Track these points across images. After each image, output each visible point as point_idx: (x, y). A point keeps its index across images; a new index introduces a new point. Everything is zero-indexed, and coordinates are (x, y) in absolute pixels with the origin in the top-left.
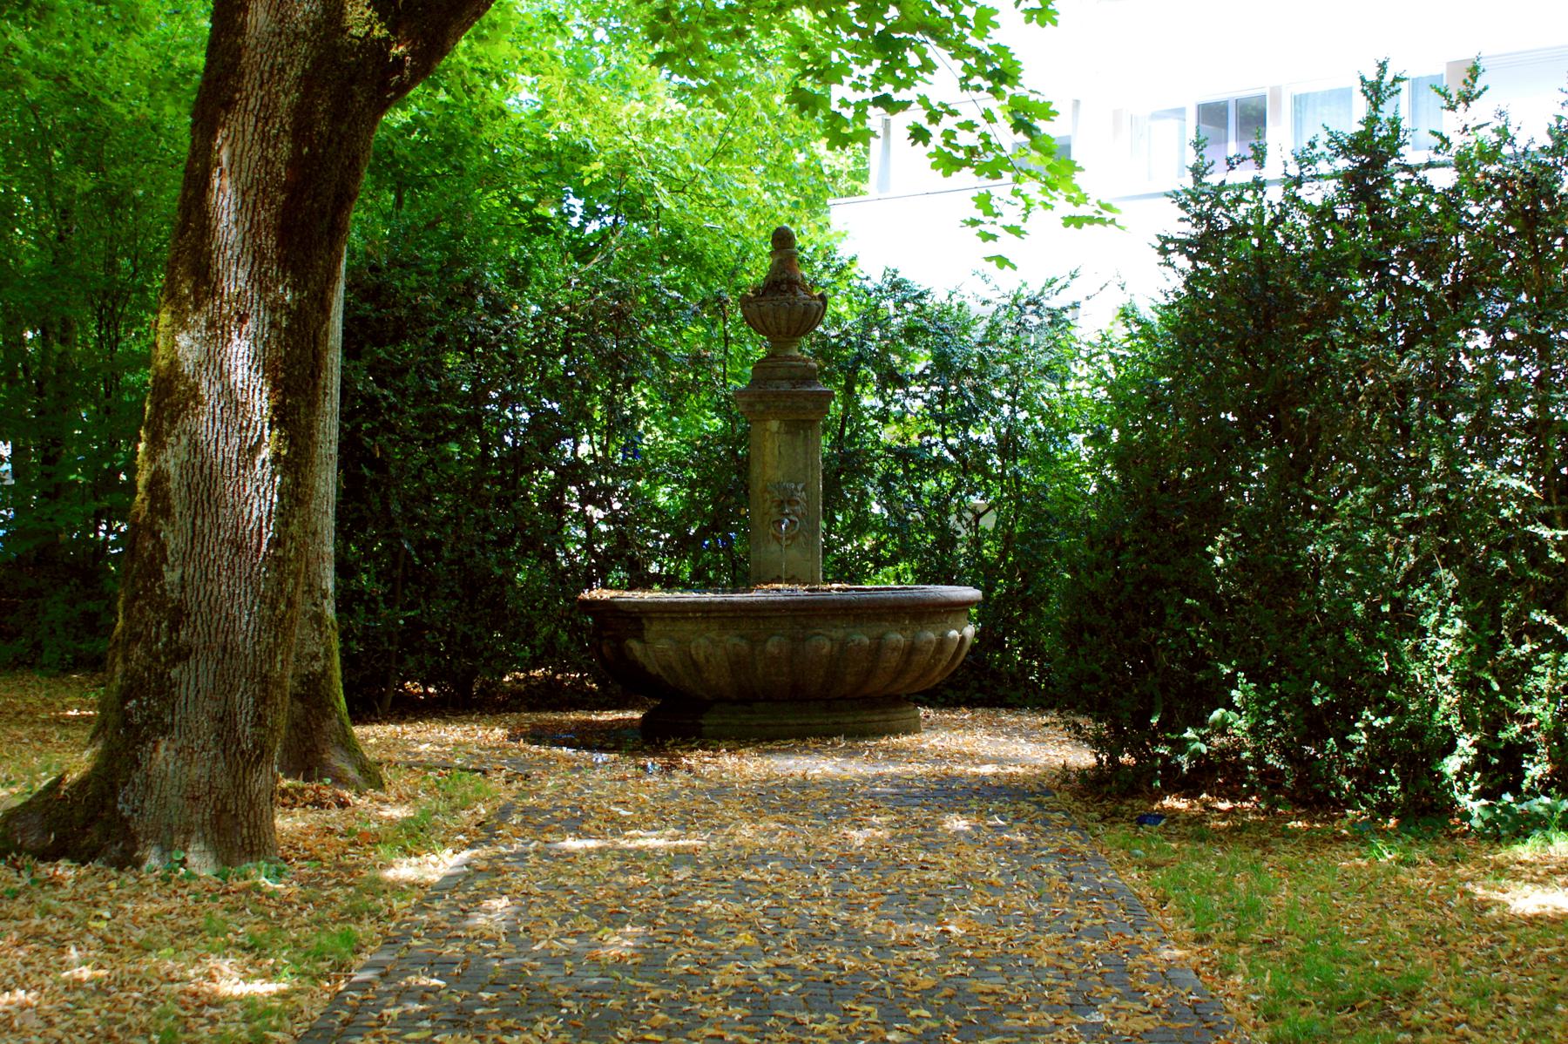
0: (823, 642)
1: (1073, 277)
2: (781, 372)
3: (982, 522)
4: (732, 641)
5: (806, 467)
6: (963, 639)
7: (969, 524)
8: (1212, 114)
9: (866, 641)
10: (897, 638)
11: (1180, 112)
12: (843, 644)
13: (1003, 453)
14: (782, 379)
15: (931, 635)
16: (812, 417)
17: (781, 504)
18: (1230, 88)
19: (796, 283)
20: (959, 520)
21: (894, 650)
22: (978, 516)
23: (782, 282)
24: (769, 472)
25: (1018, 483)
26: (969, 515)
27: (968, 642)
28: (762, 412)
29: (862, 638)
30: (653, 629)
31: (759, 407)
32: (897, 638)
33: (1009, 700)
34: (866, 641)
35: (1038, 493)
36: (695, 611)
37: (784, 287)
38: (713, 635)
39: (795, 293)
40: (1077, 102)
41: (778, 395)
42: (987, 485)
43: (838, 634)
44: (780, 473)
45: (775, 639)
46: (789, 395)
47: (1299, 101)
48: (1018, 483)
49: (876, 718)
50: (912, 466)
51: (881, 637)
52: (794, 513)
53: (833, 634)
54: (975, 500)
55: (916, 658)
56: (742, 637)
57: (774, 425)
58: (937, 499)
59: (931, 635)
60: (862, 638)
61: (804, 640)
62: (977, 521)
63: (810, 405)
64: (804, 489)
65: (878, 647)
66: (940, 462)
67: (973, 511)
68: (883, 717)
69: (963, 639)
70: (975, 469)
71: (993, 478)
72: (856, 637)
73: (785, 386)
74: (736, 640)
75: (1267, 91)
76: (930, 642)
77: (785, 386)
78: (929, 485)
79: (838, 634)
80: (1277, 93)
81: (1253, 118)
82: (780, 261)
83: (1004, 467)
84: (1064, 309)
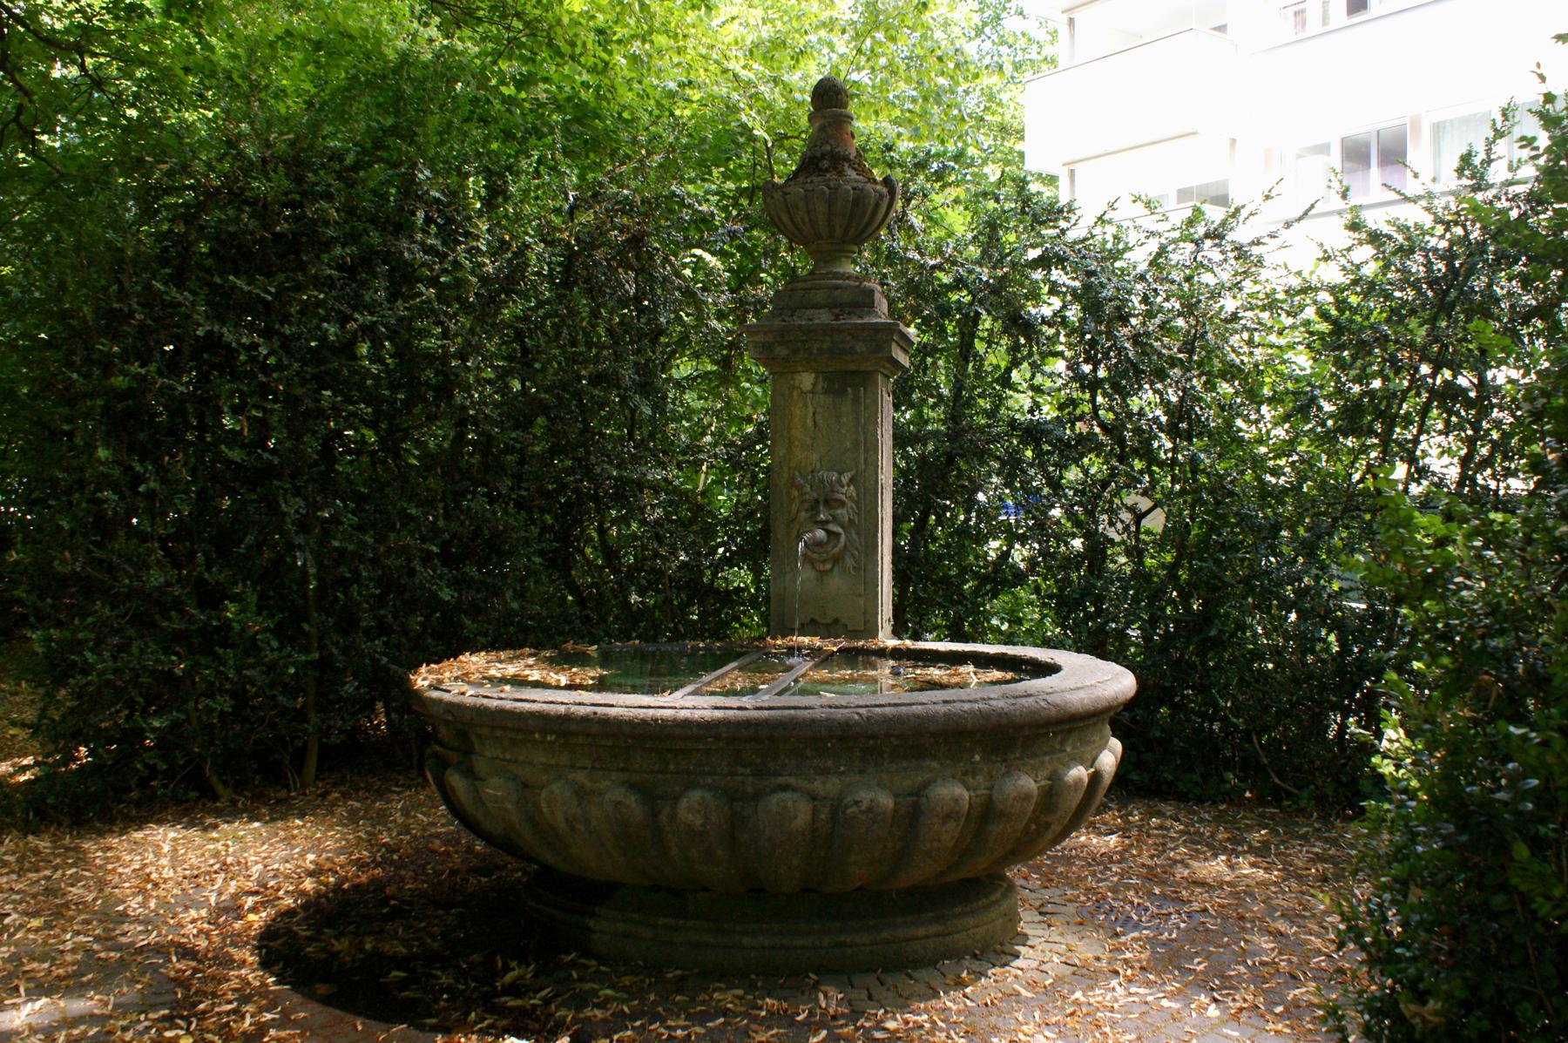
0: (791, 808)
1: (1267, 197)
2: (819, 297)
3: (1145, 523)
4: (615, 795)
5: (856, 445)
6: (1096, 777)
7: (1127, 528)
8: (1356, 154)
9: (886, 801)
10: (953, 792)
11: (1324, 149)
12: (838, 806)
13: (1172, 431)
14: (817, 307)
15: (1028, 783)
16: (866, 366)
17: (814, 506)
18: (1366, 122)
19: (846, 159)
20: (1111, 524)
21: (947, 817)
22: (1139, 517)
23: (823, 156)
24: (799, 454)
25: (1194, 471)
26: (1126, 516)
27: (1107, 779)
28: (786, 359)
29: (877, 796)
30: (487, 753)
31: (781, 351)
32: (953, 792)
33: (1181, 787)
34: (886, 801)
35: (1219, 488)
36: (544, 732)
37: (825, 164)
38: (581, 777)
39: (841, 173)
40: (1234, 141)
41: (809, 331)
42: (1151, 474)
43: (828, 786)
44: (815, 457)
45: (696, 795)
46: (828, 331)
47: (1438, 129)
48: (1194, 471)
49: (921, 931)
50: (1046, 447)
51: (918, 792)
52: (835, 519)
53: (818, 786)
54: (1131, 498)
55: (995, 829)
56: (632, 786)
57: (807, 380)
58: (1083, 493)
59: (1028, 783)
60: (877, 796)
61: (758, 796)
62: (1138, 524)
63: (860, 347)
64: (852, 481)
65: (912, 813)
66: (1085, 444)
67: (1131, 509)
68: (936, 928)
69: (1096, 777)
70: (1135, 452)
71: (1161, 464)
72: (865, 796)
73: (824, 317)
74: (618, 793)
75: (1407, 120)
76: (1027, 797)
77: (824, 317)
78: (1073, 474)
79: (828, 786)
80: (1416, 123)
81: (1393, 155)
82: (822, 129)
83: (1175, 450)
84: (1257, 243)
